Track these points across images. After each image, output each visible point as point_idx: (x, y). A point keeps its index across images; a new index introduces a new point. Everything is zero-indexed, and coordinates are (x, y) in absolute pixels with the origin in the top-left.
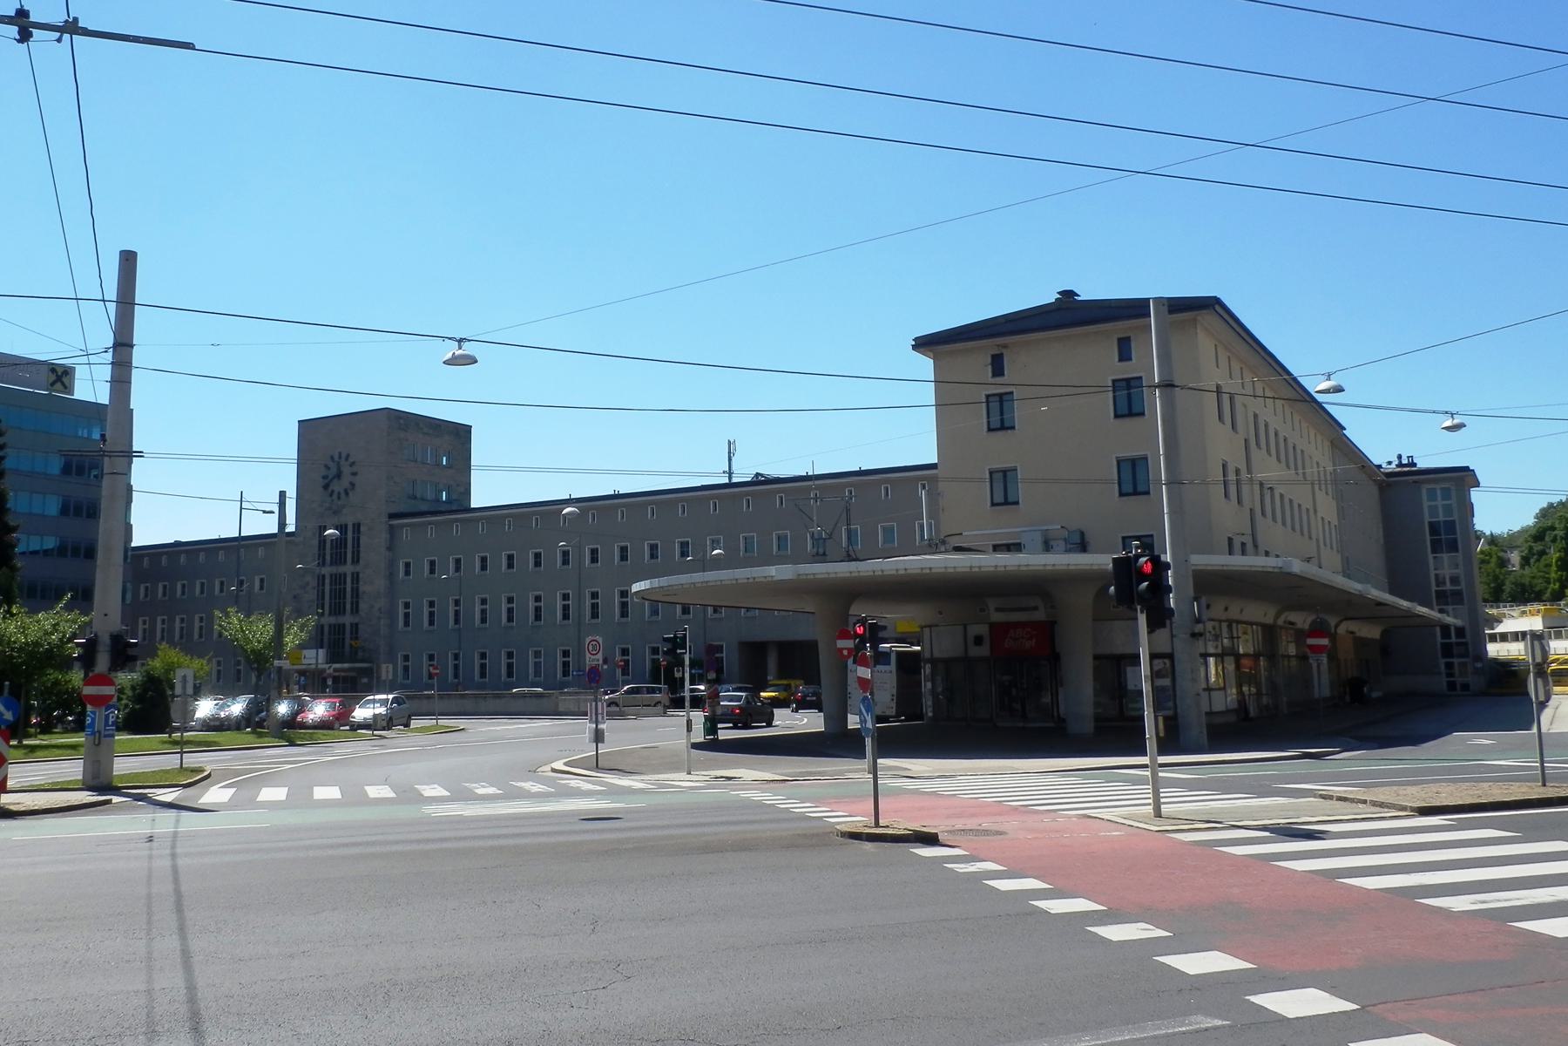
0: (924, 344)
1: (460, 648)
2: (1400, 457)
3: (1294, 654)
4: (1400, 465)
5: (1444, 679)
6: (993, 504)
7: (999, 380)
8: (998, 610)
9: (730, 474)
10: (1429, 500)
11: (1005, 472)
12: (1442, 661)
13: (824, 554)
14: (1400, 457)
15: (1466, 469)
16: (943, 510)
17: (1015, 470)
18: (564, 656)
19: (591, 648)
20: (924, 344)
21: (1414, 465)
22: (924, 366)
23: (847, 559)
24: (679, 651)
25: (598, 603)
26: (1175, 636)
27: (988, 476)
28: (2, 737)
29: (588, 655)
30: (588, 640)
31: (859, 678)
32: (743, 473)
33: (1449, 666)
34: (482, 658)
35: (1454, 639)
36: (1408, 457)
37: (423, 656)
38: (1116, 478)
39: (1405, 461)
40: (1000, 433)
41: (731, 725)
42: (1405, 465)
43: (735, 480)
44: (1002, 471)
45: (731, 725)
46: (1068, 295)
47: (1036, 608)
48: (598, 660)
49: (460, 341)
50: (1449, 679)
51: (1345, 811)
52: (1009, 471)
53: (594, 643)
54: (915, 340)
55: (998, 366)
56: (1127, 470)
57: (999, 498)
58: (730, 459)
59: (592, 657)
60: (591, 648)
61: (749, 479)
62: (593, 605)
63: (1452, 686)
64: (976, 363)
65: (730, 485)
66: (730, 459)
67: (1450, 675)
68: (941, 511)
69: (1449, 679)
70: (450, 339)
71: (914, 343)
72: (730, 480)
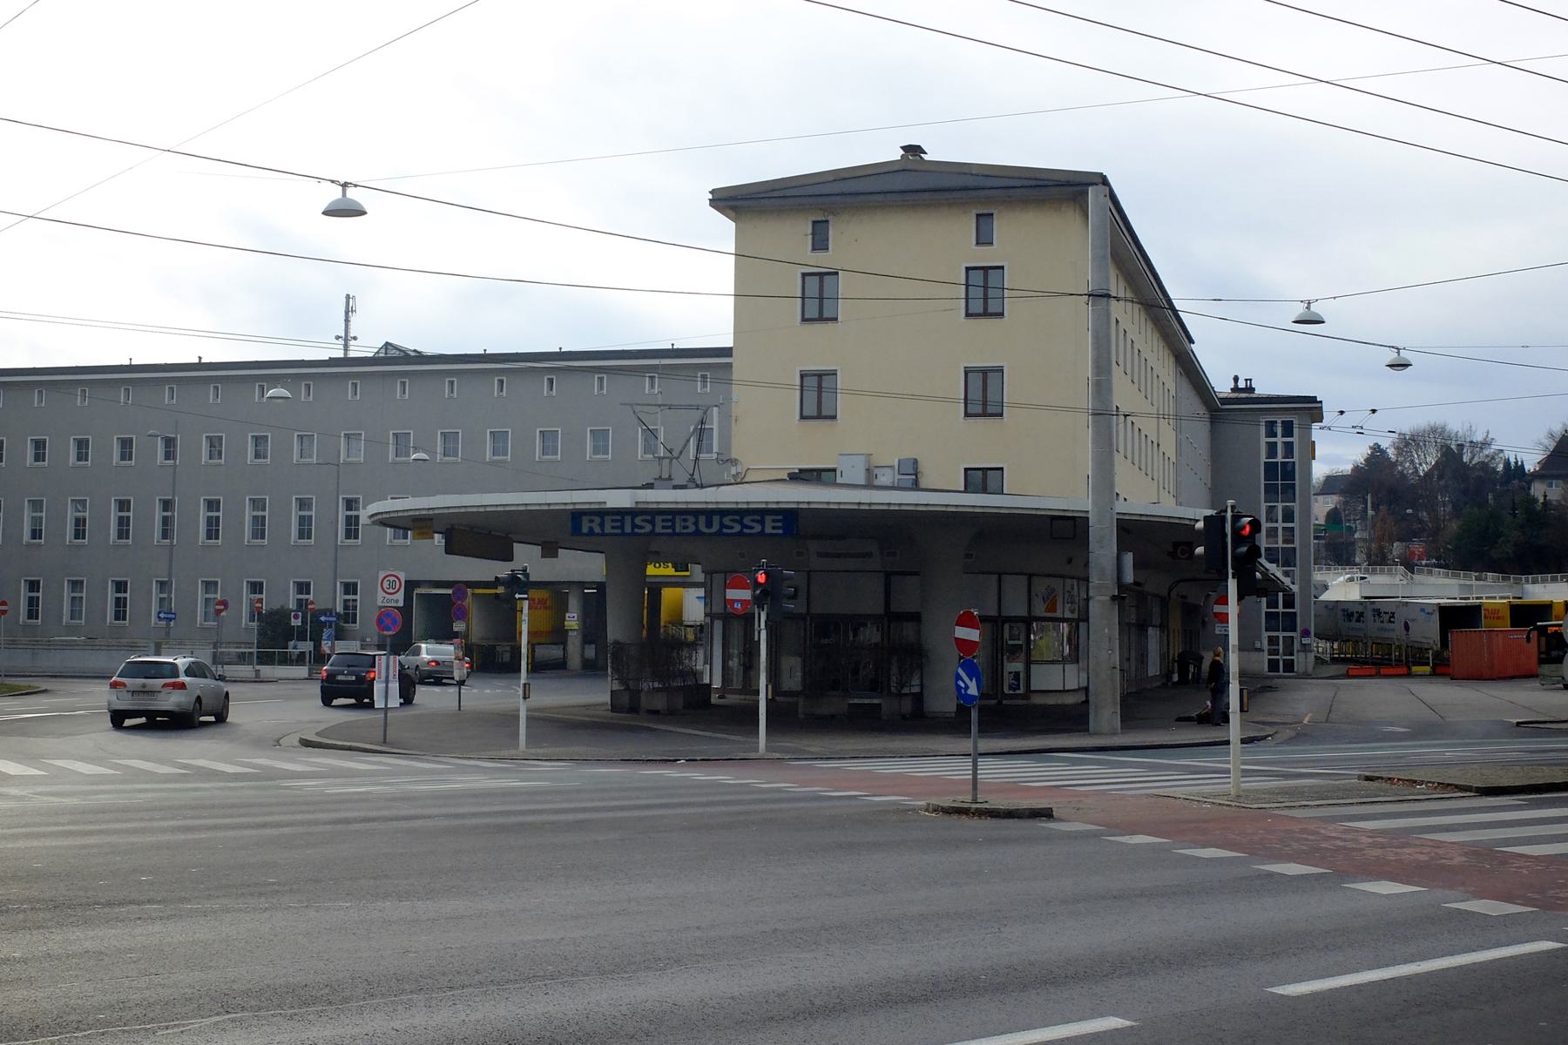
0: (729, 201)
1: (170, 576)
2: (1236, 379)
3: (1134, 621)
4: (1236, 389)
5: (1266, 657)
6: (802, 417)
7: (820, 255)
8: (820, 555)
9: (347, 339)
10: (1268, 436)
11: (820, 375)
12: (1266, 635)
13: (670, 478)
14: (1236, 379)
15: (1313, 399)
16: (736, 420)
17: (834, 373)
18: (118, 591)
19: (386, 584)
20: (729, 201)
21: (1251, 390)
22: (724, 229)
23: (691, 484)
24: (517, 596)
25: (128, 518)
26: (1092, 598)
27: (798, 382)
28: (1565, 642)
29: (380, 594)
30: (382, 575)
31: (956, 639)
32: (365, 347)
33: (1273, 641)
34: (31, 590)
35: (1281, 609)
36: (1246, 380)
37: (21, 582)
38: (963, 397)
39: (1242, 384)
40: (818, 327)
41: (352, 701)
42: (1242, 390)
43: (352, 354)
44: (814, 375)
45: (352, 701)
46: (913, 150)
47: (869, 555)
48: (397, 601)
49: (345, 185)
50: (1271, 657)
51: (1406, 792)
52: (825, 375)
53: (392, 579)
54: (712, 192)
55: (820, 243)
56: (976, 381)
57: (811, 409)
58: (347, 321)
59: (388, 596)
60: (386, 584)
61: (371, 355)
62: (121, 519)
63: (1273, 665)
64: (792, 236)
65: (346, 361)
66: (347, 321)
67: (1274, 652)
68: (733, 421)
69: (1271, 657)
70: (333, 182)
71: (710, 197)
72: (345, 354)
